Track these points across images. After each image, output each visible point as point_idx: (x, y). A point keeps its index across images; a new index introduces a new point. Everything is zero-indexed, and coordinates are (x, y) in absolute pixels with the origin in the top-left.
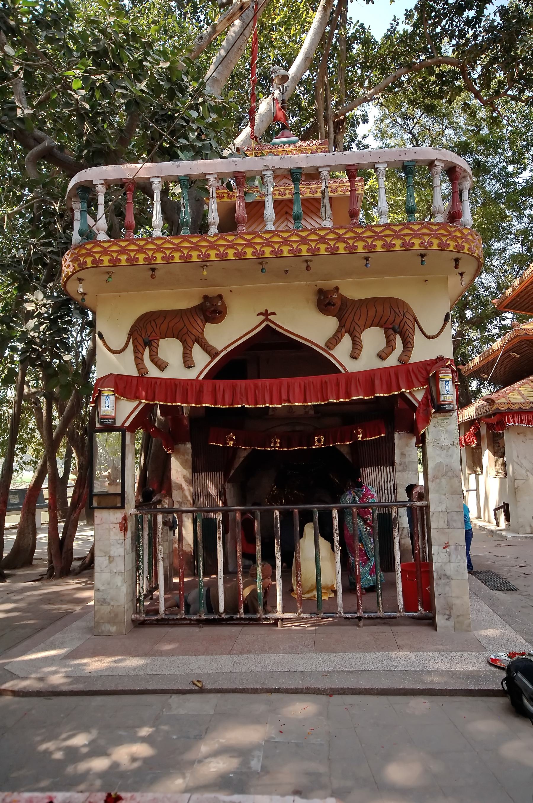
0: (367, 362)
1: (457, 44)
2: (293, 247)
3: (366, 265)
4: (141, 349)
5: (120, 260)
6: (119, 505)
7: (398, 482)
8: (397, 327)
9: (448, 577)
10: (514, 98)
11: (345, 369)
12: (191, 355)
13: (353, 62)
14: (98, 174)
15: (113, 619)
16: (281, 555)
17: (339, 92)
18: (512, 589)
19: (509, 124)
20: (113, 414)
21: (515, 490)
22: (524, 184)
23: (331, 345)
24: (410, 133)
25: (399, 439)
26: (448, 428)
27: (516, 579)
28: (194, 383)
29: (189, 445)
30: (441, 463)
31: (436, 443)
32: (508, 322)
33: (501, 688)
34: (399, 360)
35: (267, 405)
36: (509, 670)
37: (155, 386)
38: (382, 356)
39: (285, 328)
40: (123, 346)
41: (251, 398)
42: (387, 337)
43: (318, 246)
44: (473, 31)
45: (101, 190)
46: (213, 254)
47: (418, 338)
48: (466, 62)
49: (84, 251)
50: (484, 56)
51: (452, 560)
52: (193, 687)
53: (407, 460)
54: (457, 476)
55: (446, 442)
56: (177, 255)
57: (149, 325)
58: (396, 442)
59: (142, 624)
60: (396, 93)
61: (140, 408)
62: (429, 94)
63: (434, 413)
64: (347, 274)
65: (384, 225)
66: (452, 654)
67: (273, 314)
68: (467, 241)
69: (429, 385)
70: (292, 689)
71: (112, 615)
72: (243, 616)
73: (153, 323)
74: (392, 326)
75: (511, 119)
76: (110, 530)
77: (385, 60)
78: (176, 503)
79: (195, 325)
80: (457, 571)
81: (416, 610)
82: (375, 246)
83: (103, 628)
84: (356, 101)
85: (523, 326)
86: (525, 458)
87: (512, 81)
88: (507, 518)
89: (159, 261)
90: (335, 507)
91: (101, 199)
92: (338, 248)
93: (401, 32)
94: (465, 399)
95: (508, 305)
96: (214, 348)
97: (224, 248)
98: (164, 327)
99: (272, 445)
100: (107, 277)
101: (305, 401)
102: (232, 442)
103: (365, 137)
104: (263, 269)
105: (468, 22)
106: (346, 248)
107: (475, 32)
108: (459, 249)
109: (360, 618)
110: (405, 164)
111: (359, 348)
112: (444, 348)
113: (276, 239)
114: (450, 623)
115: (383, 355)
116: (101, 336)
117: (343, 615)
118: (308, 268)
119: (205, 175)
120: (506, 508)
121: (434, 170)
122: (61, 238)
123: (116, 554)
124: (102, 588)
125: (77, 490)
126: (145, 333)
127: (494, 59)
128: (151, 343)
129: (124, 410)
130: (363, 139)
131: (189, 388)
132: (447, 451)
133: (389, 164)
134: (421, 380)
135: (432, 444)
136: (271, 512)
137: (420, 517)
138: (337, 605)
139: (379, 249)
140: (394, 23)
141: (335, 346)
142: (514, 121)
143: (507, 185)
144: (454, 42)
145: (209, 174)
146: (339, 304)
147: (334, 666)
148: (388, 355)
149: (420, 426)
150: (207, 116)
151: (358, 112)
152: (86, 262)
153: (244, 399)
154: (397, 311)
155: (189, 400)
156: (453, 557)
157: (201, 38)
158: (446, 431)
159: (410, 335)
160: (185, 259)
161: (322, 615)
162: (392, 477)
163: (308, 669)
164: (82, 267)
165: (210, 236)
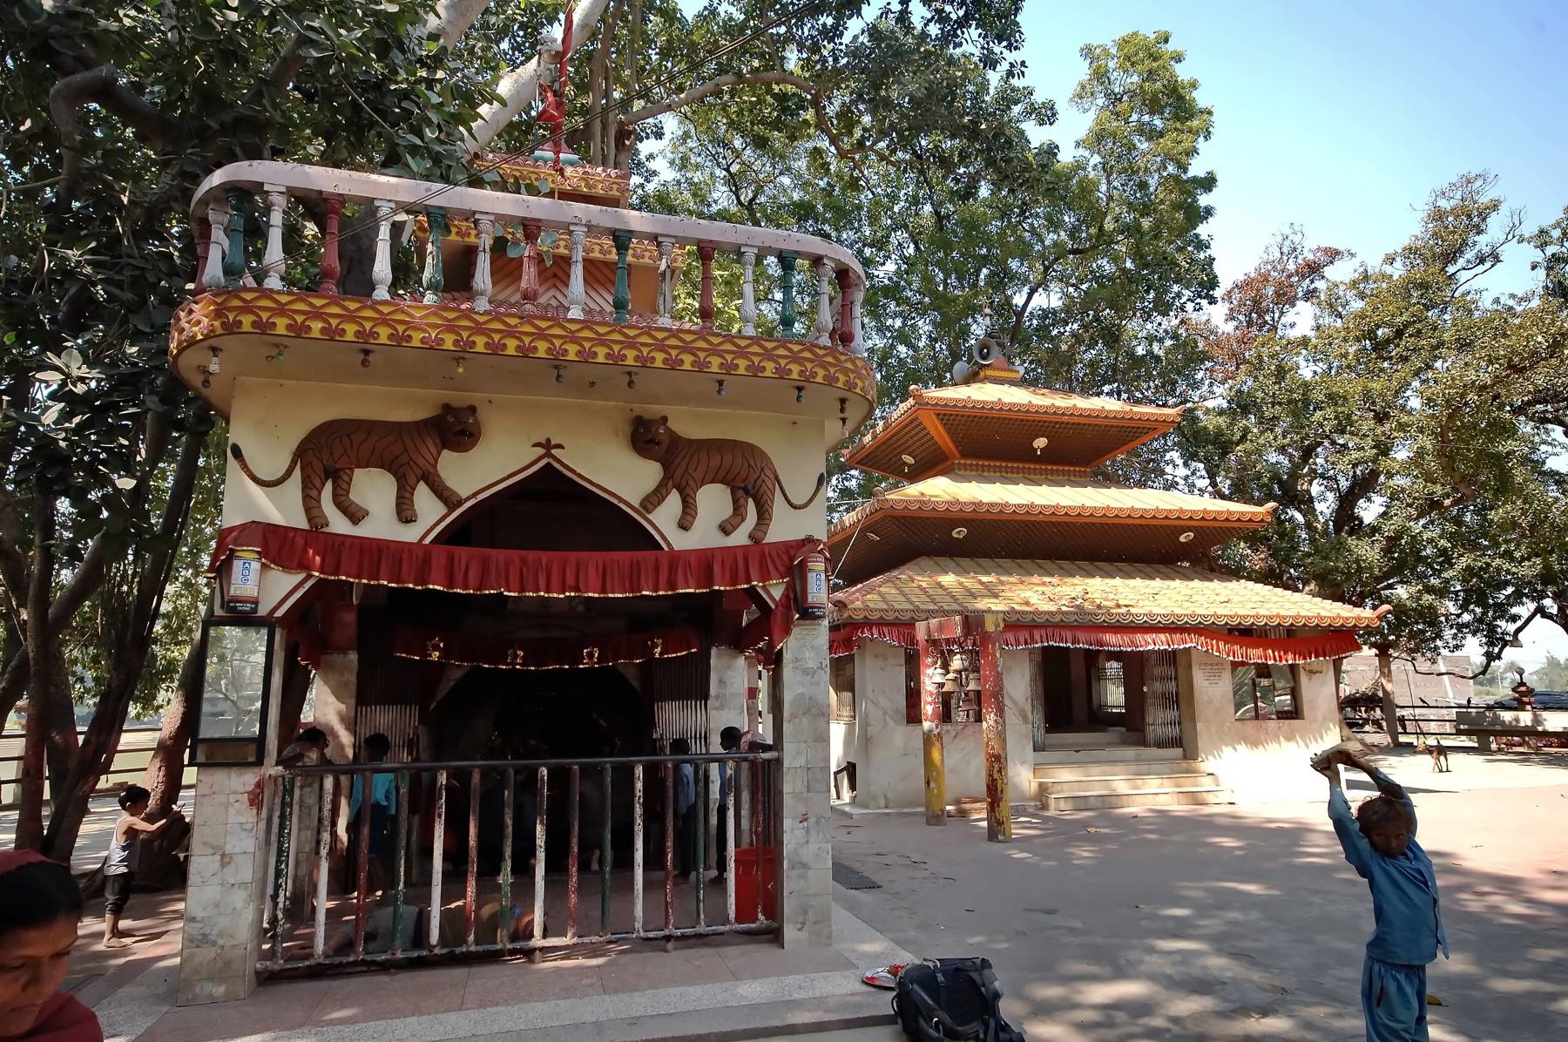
0: (704, 536)
1: (808, 59)
3: (719, 392)
4: (318, 483)
5: (309, 328)
6: (252, 759)
9: (804, 866)
11: (669, 544)
14: (275, 175)
15: (223, 970)
17: (625, 85)
18: (872, 886)
24: (727, 170)
29: (353, 657)
32: (853, 484)
36: (901, 984)
38: (725, 529)
42: (735, 501)
46: (480, 342)
47: (779, 507)
49: (236, 303)
55: (811, 664)
57: (337, 442)
58: (713, 661)
59: (267, 979)
60: (710, 105)
64: (681, 398)
65: (750, 338)
67: (560, 446)
68: (860, 377)
71: (220, 964)
72: (473, 948)
73: (346, 441)
76: (228, 805)
79: (423, 450)
81: (755, 919)
83: (197, 990)
84: (659, 108)
88: (853, 787)
89: (383, 339)
96: (454, 493)
101: (604, 591)
103: (651, 157)
104: (559, 376)
108: (850, 386)
109: (668, 938)
114: (803, 935)
115: (728, 527)
117: (642, 934)
118: (631, 384)
119: (475, 213)
120: (850, 769)
121: (821, 270)
123: (237, 850)
124: (200, 914)
125: (93, 739)
126: (326, 457)
128: (339, 477)
129: (271, 587)
133: (760, 249)
134: (781, 569)
136: (535, 771)
138: (634, 919)
139: (742, 371)
146: (664, 447)
148: (735, 528)
156: (813, 834)
163: (603, 1018)
164: (231, 329)
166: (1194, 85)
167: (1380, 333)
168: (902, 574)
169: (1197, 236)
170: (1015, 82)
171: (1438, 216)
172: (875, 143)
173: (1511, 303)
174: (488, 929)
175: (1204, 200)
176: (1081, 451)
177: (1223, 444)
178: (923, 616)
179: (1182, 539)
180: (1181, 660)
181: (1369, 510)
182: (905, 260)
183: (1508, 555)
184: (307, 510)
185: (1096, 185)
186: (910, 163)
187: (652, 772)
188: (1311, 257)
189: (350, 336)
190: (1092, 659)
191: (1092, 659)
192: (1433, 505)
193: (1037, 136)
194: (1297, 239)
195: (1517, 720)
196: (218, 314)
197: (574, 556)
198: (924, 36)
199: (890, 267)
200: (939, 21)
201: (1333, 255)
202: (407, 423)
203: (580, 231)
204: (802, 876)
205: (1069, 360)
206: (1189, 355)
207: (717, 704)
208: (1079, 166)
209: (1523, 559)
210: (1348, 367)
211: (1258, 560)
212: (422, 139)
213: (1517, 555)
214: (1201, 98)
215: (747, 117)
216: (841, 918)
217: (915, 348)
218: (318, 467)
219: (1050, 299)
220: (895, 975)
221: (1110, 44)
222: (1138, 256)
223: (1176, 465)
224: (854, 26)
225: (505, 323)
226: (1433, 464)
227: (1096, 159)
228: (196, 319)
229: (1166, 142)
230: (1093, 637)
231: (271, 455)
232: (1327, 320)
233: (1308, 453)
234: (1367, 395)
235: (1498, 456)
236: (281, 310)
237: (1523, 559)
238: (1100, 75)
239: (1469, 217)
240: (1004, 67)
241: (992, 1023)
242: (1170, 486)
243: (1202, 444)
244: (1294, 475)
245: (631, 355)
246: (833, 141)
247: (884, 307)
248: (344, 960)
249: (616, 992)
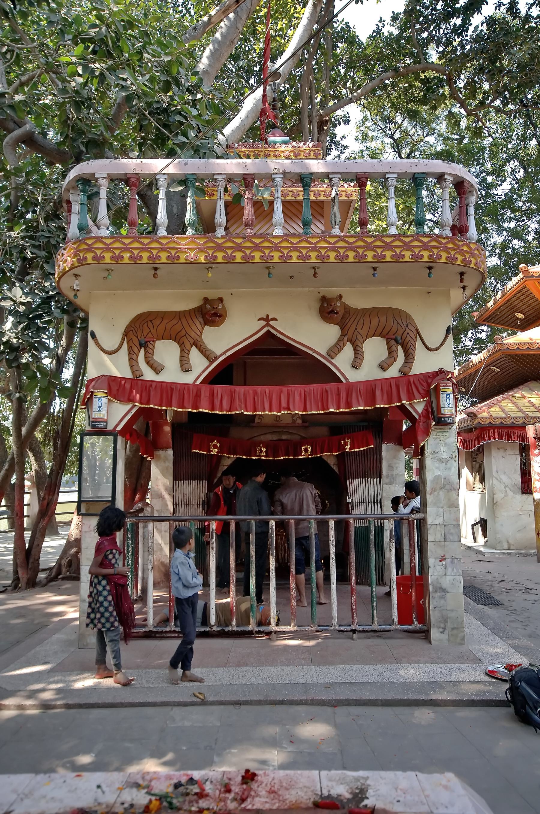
0: (369, 372)
1: (444, 51)
2: (302, 253)
3: (374, 275)
4: (136, 350)
5: (123, 257)
7: (385, 495)
8: (399, 338)
9: (444, 590)
10: (498, 110)
11: (346, 378)
12: (188, 358)
13: (338, 61)
14: (97, 167)
16: (276, 568)
17: (323, 91)
19: (490, 135)
20: (106, 417)
22: (503, 197)
23: (332, 354)
24: (392, 137)
25: (387, 450)
26: (448, 441)
27: (500, 594)
28: (191, 387)
29: (170, 452)
30: (439, 475)
31: (434, 456)
32: (483, 336)
33: (505, 699)
34: (400, 371)
35: (267, 412)
36: (512, 681)
37: (149, 391)
38: (383, 367)
39: (287, 334)
40: (116, 346)
42: (389, 348)
43: (327, 254)
44: (460, 39)
46: (220, 256)
47: (419, 350)
48: (453, 71)
49: (84, 247)
50: (469, 65)
51: (448, 573)
52: (195, 699)
54: (454, 489)
55: (445, 456)
57: (145, 325)
60: (380, 96)
61: (133, 411)
63: (434, 425)
65: (394, 236)
66: (449, 665)
67: (274, 319)
68: (474, 256)
69: (430, 397)
70: (296, 701)
72: (235, 629)
73: (150, 324)
74: (394, 337)
75: (491, 130)
77: (369, 61)
78: (155, 512)
79: (194, 328)
80: (453, 584)
81: (411, 623)
82: (385, 256)
83: (88, 641)
84: (343, 102)
86: (505, 473)
87: (498, 93)
88: (485, 535)
90: (332, 518)
91: (103, 193)
92: (347, 256)
93: (386, 34)
95: (488, 318)
96: (212, 352)
97: (231, 251)
98: (161, 328)
99: (257, 453)
100: (106, 274)
102: (216, 450)
104: (269, 273)
105: (456, 31)
106: (355, 257)
107: (462, 40)
108: (466, 263)
109: (354, 631)
110: (416, 176)
111: (361, 357)
112: (444, 360)
113: (285, 244)
114: (445, 636)
115: (385, 365)
116: (93, 336)
117: (337, 627)
119: (214, 174)
120: (483, 523)
121: (444, 184)
122: (43, 231)
126: (141, 334)
127: (481, 69)
129: (115, 413)
130: (342, 139)
131: (185, 393)
132: (446, 464)
133: (399, 174)
135: (431, 457)
136: (267, 523)
138: (331, 618)
139: (388, 259)
140: (380, 25)
141: (336, 355)
142: (494, 133)
144: (441, 49)
145: (218, 174)
146: (341, 313)
147: (335, 678)
148: (389, 366)
149: (420, 438)
150: (205, 113)
151: (340, 113)
152: (86, 258)
153: (243, 406)
154: (400, 322)
155: (186, 404)
156: (450, 570)
157: (195, 28)
158: (445, 444)
159: (412, 347)
162: (379, 489)
163: (309, 681)
165: (218, 238)
168: (518, 394)
172: (492, 101)
174: (244, 619)
178: (532, 421)
182: (518, 181)
186: (518, 111)
196: (76, 255)
198: (528, 17)
199: (506, 187)
202: (189, 311)
204: (442, 597)
207: (387, 481)
212: (188, 139)
216: (472, 626)
217: (525, 241)
220: (510, 671)
224: (477, 20)
225: (234, 242)
228: (65, 259)
236: (108, 248)
245: (313, 255)
246: (462, 106)
247: (503, 215)
248: (164, 630)
249: (319, 664)
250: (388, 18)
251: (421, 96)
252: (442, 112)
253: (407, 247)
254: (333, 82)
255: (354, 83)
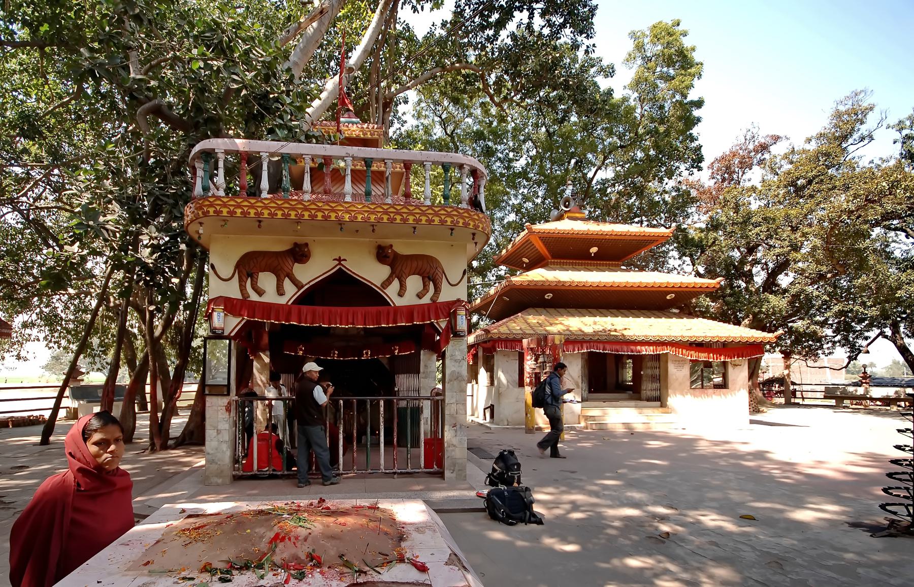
0: (409, 299)
14: (218, 144)
15: (220, 474)
21: (499, 394)
24: (440, 117)
25: (424, 355)
32: (502, 273)
38: (420, 296)
41: (326, 320)
45: (221, 157)
47: (444, 285)
49: (207, 203)
53: (429, 370)
55: (459, 358)
56: (280, 213)
59: (236, 478)
62: (456, 89)
67: (345, 260)
68: (481, 222)
77: (424, 57)
81: (432, 468)
84: (405, 88)
85: (514, 279)
89: (266, 216)
93: (437, 35)
94: (472, 327)
105: (488, 39)
109: (395, 473)
112: (461, 293)
114: (454, 475)
120: (492, 408)
124: (211, 452)
126: (248, 267)
128: (253, 275)
137: (438, 407)
139: (423, 222)
143: (508, 168)
144: (477, 53)
146: (392, 257)
149: (442, 345)
156: (459, 433)
160: (286, 216)
161: (370, 471)
164: (206, 214)
166: (693, 49)
167: (799, 182)
169: (691, 134)
170: (593, 56)
171: (838, 115)
173: (879, 163)
175: (696, 113)
176: (615, 253)
177: (700, 246)
179: (668, 297)
180: (662, 359)
181: (784, 280)
183: (863, 304)
184: (241, 291)
185: (634, 109)
187: (389, 405)
188: (763, 141)
189: (252, 215)
190: (619, 360)
191: (619, 360)
192: (822, 277)
193: (603, 83)
194: (755, 131)
195: (856, 391)
197: (352, 309)
198: (540, 35)
200: (550, 26)
201: (776, 139)
203: (349, 160)
205: (617, 206)
206: (685, 200)
208: (625, 99)
209: (871, 306)
210: (779, 202)
211: (713, 306)
213: (869, 304)
214: (697, 57)
215: (449, 88)
218: (245, 273)
219: (607, 174)
221: (646, 29)
222: (656, 146)
223: (674, 258)
224: (504, 34)
226: (820, 254)
227: (636, 95)
228: (189, 211)
229: (675, 82)
230: (614, 347)
231: (226, 268)
232: (770, 177)
233: (751, 250)
234: (787, 217)
235: (859, 249)
236: (225, 205)
237: (871, 306)
238: (640, 47)
239: (856, 114)
240: (582, 49)
241: (528, 513)
242: (669, 271)
243: (687, 245)
244: (743, 262)
250: (439, 25)
251: (461, 89)
252: (477, 101)
253: (436, 214)
254: (395, 69)
255: (412, 72)
